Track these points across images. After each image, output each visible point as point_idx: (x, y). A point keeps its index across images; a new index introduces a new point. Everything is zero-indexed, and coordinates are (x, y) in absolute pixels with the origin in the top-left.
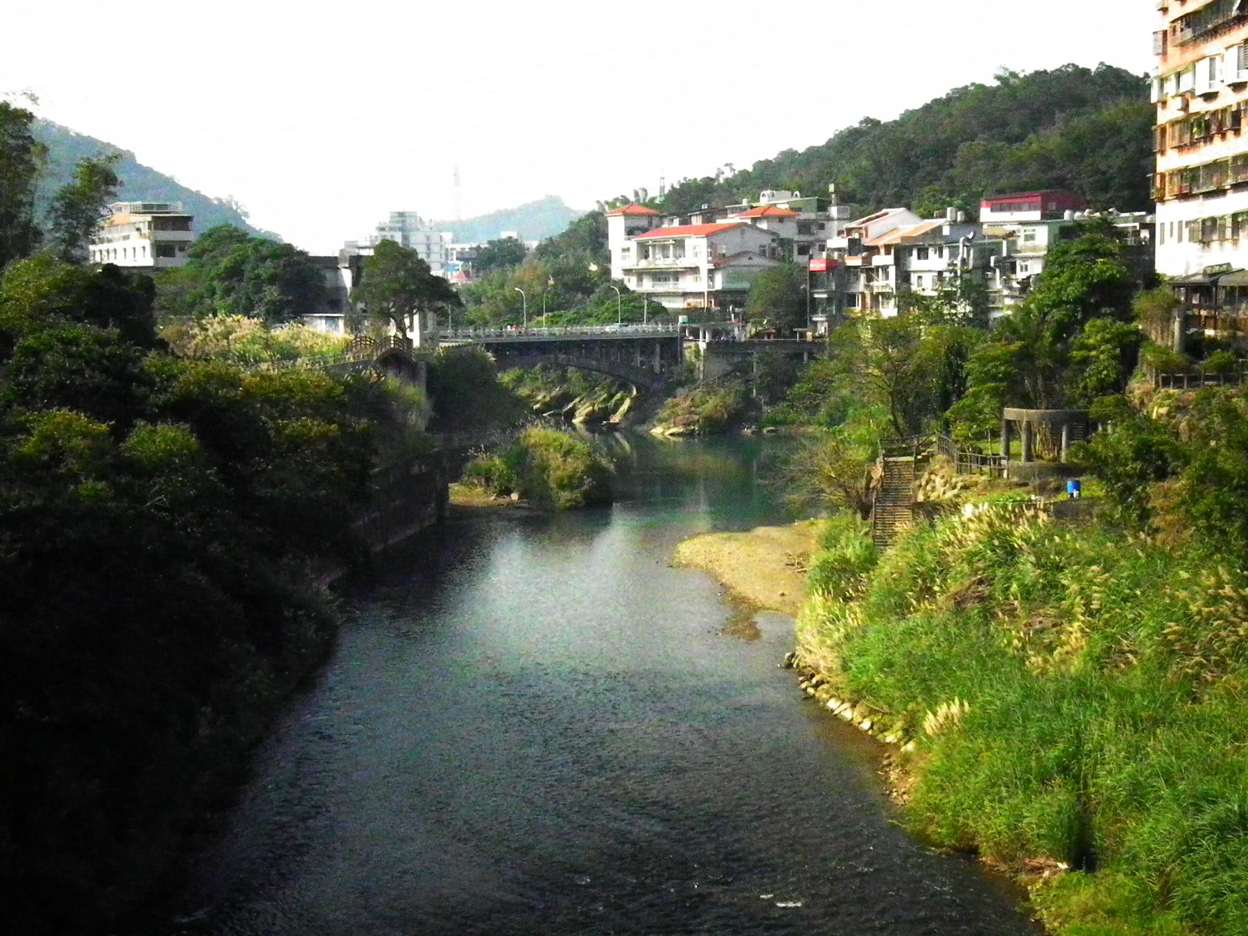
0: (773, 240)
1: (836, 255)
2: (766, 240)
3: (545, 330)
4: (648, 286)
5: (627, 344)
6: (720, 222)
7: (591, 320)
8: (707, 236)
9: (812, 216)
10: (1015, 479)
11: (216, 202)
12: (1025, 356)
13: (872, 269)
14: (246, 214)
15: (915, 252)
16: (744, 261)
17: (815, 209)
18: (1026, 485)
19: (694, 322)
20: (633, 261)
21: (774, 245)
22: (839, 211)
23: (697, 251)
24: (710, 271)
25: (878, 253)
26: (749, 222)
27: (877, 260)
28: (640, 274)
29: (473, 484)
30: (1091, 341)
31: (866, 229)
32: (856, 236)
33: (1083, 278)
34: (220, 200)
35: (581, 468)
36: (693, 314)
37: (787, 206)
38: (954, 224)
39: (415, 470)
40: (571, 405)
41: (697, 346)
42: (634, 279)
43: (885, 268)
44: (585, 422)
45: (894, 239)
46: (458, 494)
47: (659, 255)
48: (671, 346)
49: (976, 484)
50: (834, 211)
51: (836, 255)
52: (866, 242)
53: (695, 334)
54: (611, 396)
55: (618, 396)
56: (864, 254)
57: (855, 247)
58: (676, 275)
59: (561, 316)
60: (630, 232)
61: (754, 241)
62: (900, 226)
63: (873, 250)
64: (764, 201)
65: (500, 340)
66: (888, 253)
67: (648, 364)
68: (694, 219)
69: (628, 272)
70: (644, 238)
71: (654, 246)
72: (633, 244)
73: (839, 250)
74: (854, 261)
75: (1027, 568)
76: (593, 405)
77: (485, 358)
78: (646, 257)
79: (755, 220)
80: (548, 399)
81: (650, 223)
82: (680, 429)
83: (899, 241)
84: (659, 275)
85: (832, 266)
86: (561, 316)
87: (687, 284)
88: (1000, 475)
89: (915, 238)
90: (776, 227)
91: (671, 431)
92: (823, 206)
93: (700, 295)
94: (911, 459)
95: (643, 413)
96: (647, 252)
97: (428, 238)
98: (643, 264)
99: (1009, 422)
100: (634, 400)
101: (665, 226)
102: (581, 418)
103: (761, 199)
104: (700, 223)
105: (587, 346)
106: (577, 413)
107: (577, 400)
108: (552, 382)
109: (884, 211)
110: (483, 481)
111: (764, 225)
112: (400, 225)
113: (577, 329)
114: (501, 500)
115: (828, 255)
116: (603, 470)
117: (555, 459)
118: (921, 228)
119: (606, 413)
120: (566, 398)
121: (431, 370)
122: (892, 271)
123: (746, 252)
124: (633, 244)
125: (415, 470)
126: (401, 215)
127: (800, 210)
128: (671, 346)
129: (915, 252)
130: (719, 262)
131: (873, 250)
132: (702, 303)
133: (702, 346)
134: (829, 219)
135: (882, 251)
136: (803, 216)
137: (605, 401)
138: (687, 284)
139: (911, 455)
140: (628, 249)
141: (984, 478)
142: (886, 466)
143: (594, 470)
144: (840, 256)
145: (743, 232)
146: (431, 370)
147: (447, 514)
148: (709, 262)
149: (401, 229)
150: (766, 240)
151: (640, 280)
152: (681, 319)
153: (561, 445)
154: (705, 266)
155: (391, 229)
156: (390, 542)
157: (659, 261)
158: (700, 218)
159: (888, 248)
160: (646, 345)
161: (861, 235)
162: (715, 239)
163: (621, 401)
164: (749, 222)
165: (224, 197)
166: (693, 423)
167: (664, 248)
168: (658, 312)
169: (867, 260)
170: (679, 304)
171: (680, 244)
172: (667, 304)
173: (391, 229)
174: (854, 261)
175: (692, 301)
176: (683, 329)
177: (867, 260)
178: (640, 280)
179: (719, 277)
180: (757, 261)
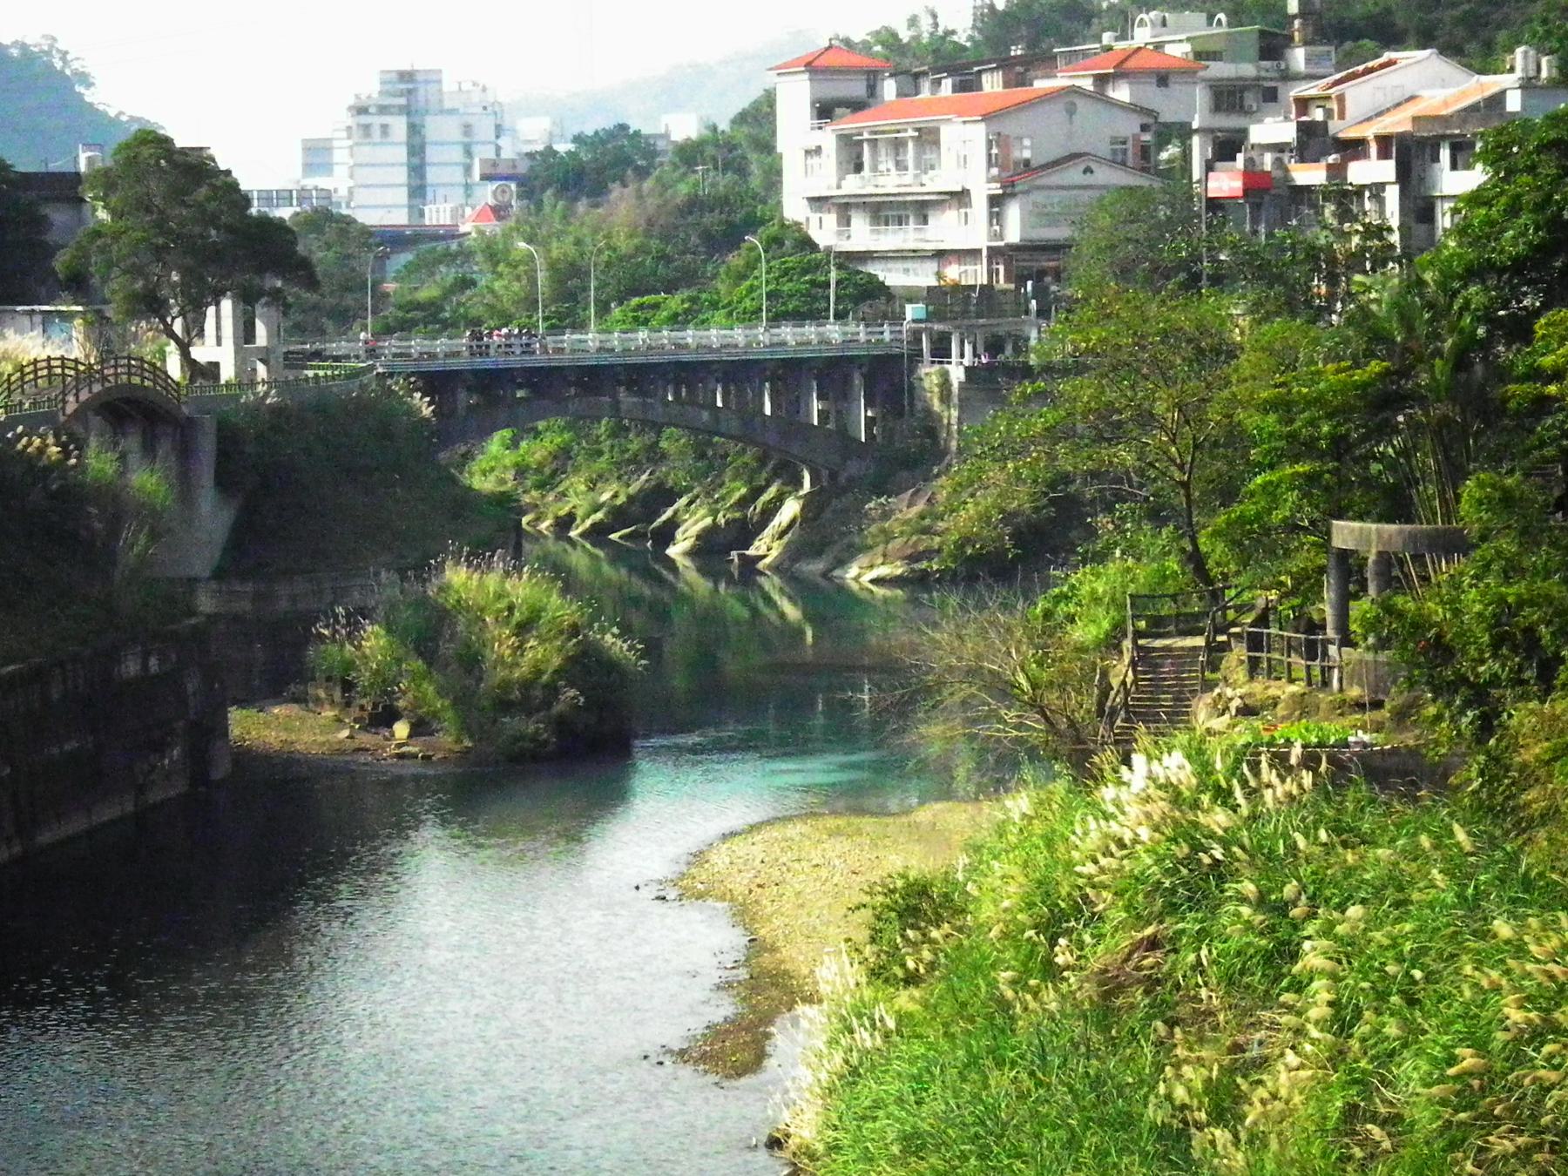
0: (1144, 128)
1: (1268, 161)
2: (1129, 127)
3: (615, 339)
4: (862, 235)
5: (789, 372)
6: (1042, 85)
7: (720, 315)
8: (987, 118)
9: (1248, 70)
10: (1354, 692)
11: (15, 52)
12: (1381, 403)
13: (1345, 194)
14: (84, 79)
15: (1445, 154)
16: (1074, 175)
17: (1253, 51)
18: (1377, 705)
19: (942, 319)
20: (826, 177)
21: (1147, 137)
22: (1308, 61)
23: (964, 155)
24: (994, 201)
25: (1366, 156)
26: (1087, 84)
27: (1361, 172)
28: (844, 208)
29: (318, 701)
30: (1547, 361)
31: (1341, 99)
32: (1318, 115)
33: (1539, 207)
34: (24, 47)
35: (556, 661)
36: (943, 300)
37: (1187, 47)
38: (1528, 85)
39: (131, 667)
40: (669, 512)
41: (945, 376)
42: (831, 219)
43: (1378, 189)
44: (691, 553)
45: (1398, 123)
46: (260, 727)
47: (886, 163)
48: (889, 376)
49: (1275, 702)
50: (1298, 57)
51: (1268, 161)
52: (1342, 129)
53: (941, 351)
54: (756, 492)
55: (772, 491)
56: (1331, 159)
57: (1312, 141)
58: (922, 209)
59: (656, 306)
60: (824, 111)
61: (1095, 130)
62: (1424, 93)
63: (1354, 149)
64: (1142, 35)
65: (480, 363)
66: (1384, 154)
67: (846, 418)
68: (986, 79)
69: (818, 202)
70: (849, 123)
71: (874, 143)
72: (827, 138)
73: (1279, 148)
74: (1310, 175)
75: (1238, 918)
76: (714, 513)
77: (412, 412)
78: (859, 168)
79: (1102, 80)
80: (621, 499)
81: (872, 90)
82: (896, 569)
83: (1407, 127)
84: (883, 211)
85: (1257, 186)
86: (656, 306)
87: (946, 230)
88: (1326, 683)
89: (1444, 120)
90: (1153, 97)
91: (874, 574)
92: (1272, 47)
93: (974, 254)
94: (1199, 641)
95: (824, 535)
96: (860, 156)
97: (467, 129)
98: (853, 185)
99: (1344, 555)
100: (809, 503)
101: (926, 92)
102: (687, 544)
103: (1138, 31)
104: (999, 88)
105: (689, 373)
106: (679, 535)
107: (684, 500)
108: (634, 460)
109: (1388, 55)
110: (337, 694)
111: (1121, 93)
112: (402, 101)
113: (690, 336)
114: (366, 739)
115: (1250, 162)
116: (610, 666)
117: (501, 643)
118: (1464, 95)
119: (746, 532)
120: (662, 495)
121: (229, 439)
122: (1392, 195)
123: (1074, 156)
124: (827, 138)
125: (131, 667)
126: (406, 76)
127: (1214, 56)
128: (889, 376)
129: (1445, 154)
130: (1014, 178)
131: (1354, 149)
132: (975, 274)
133: (957, 374)
134: (1288, 77)
135: (1373, 149)
136: (1220, 70)
137: (743, 503)
138: (946, 230)
139: (1200, 632)
140: (818, 150)
141: (1293, 688)
142: (1143, 659)
143: (587, 664)
144: (1278, 163)
145: (1071, 111)
146: (229, 439)
147: (221, 769)
148: (991, 180)
149: (407, 110)
150: (1129, 127)
151: (845, 221)
152: (912, 311)
153: (511, 608)
154: (981, 194)
155: (383, 110)
156: (45, 838)
157: (885, 180)
158: (998, 77)
159: (1384, 142)
160: (832, 372)
161: (1329, 114)
162: (1010, 127)
163: (779, 501)
164: (1087, 84)
165: (33, 39)
166: (928, 554)
167: (898, 145)
168: (866, 295)
169: (1337, 172)
170: (923, 277)
171: (928, 138)
172: (893, 277)
173: (383, 110)
174: (1310, 175)
175: (953, 272)
176: (916, 336)
177: (1337, 172)
178: (845, 221)
179: (1014, 213)
180: (1106, 176)
